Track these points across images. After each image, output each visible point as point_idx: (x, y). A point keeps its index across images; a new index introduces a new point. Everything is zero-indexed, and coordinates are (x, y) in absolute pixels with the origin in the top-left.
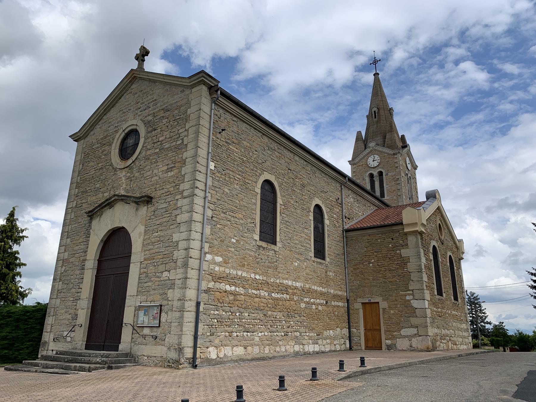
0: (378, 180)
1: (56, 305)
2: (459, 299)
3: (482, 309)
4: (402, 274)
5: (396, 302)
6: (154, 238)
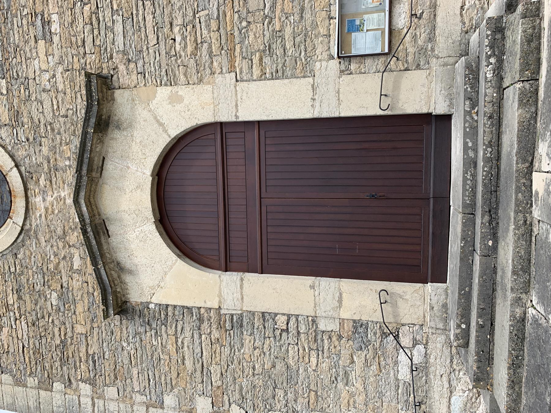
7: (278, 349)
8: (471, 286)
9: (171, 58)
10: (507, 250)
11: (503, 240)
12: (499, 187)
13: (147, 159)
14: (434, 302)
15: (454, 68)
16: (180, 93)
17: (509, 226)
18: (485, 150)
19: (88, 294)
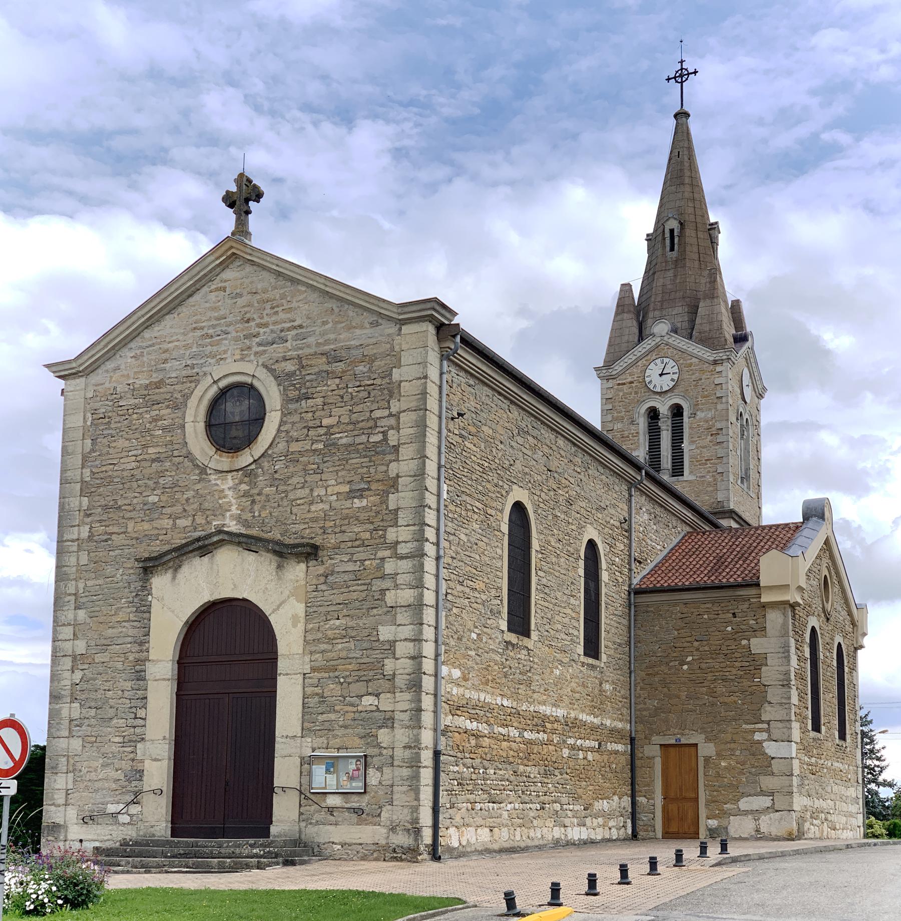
0: (670, 429)
1: (70, 751)
2: (848, 737)
3: (877, 747)
4: (750, 689)
5: (733, 746)
6: (332, 629)
16: (299, 625)
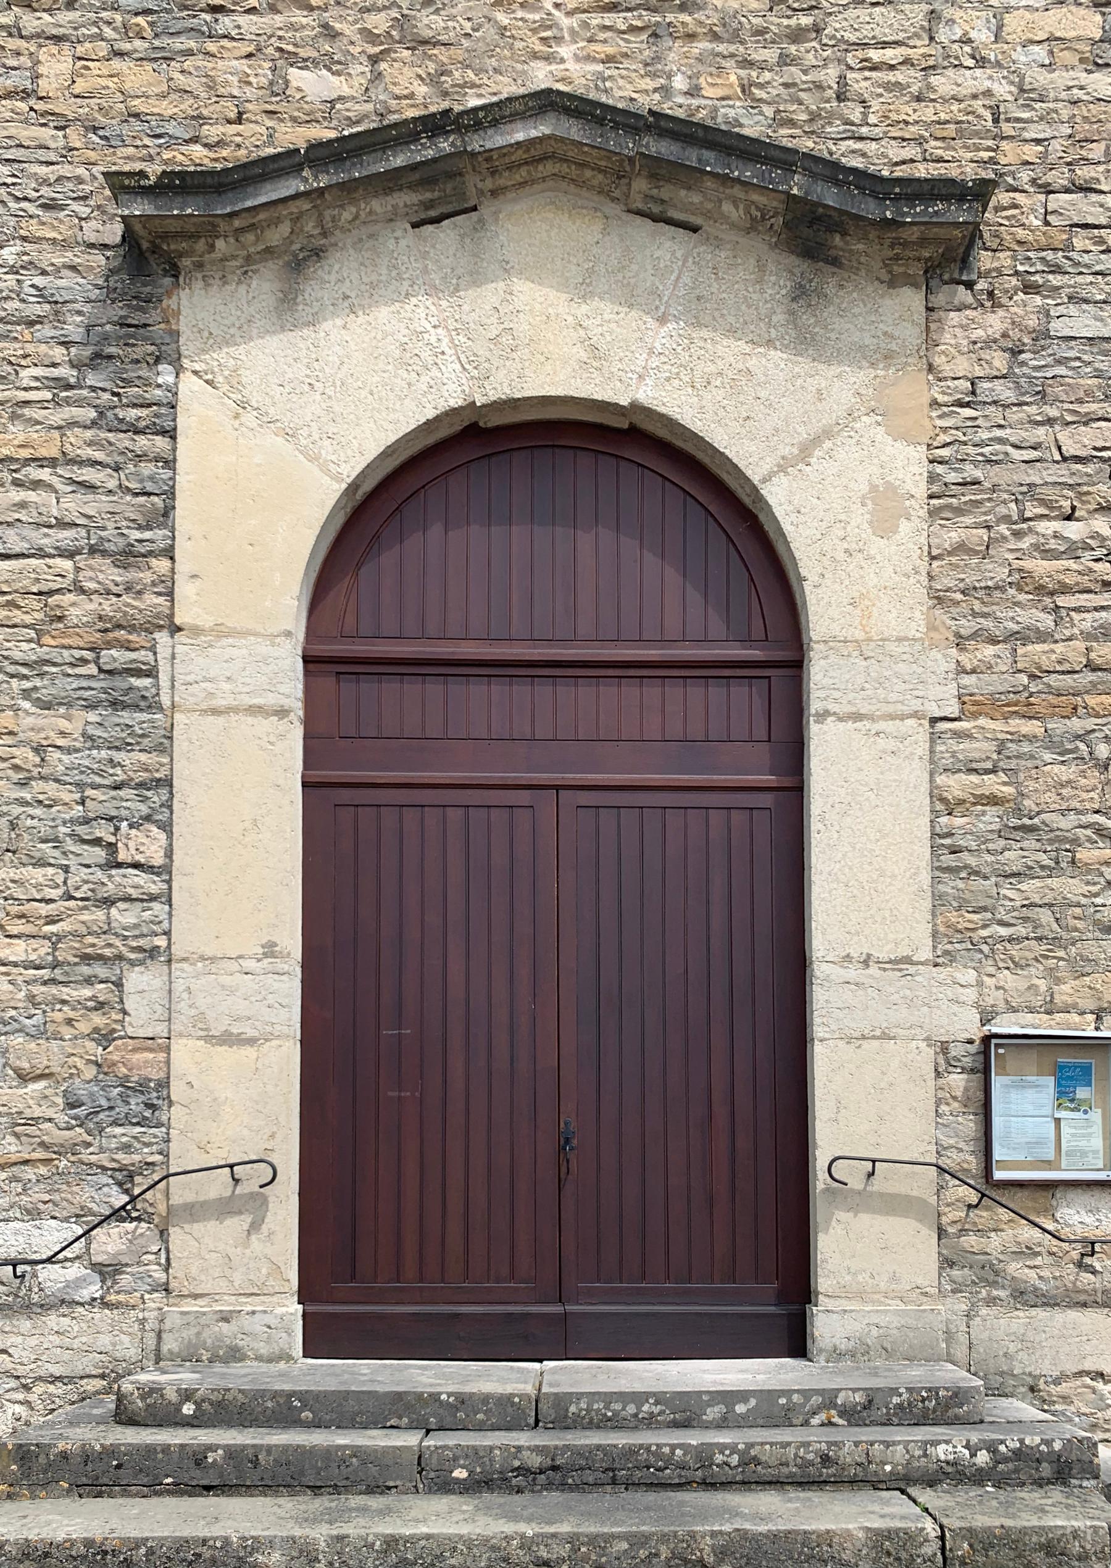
7: (45, 831)
8: (317, 1424)
9: (1016, 501)
10: (455, 1519)
11: (477, 1508)
12: (626, 1489)
13: (690, 390)
14: (246, 1322)
15: (940, 1360)
16: (905, 527)
17: (529, 1520)
18: (734, 1448)
19: (193, 118)
